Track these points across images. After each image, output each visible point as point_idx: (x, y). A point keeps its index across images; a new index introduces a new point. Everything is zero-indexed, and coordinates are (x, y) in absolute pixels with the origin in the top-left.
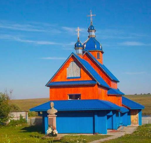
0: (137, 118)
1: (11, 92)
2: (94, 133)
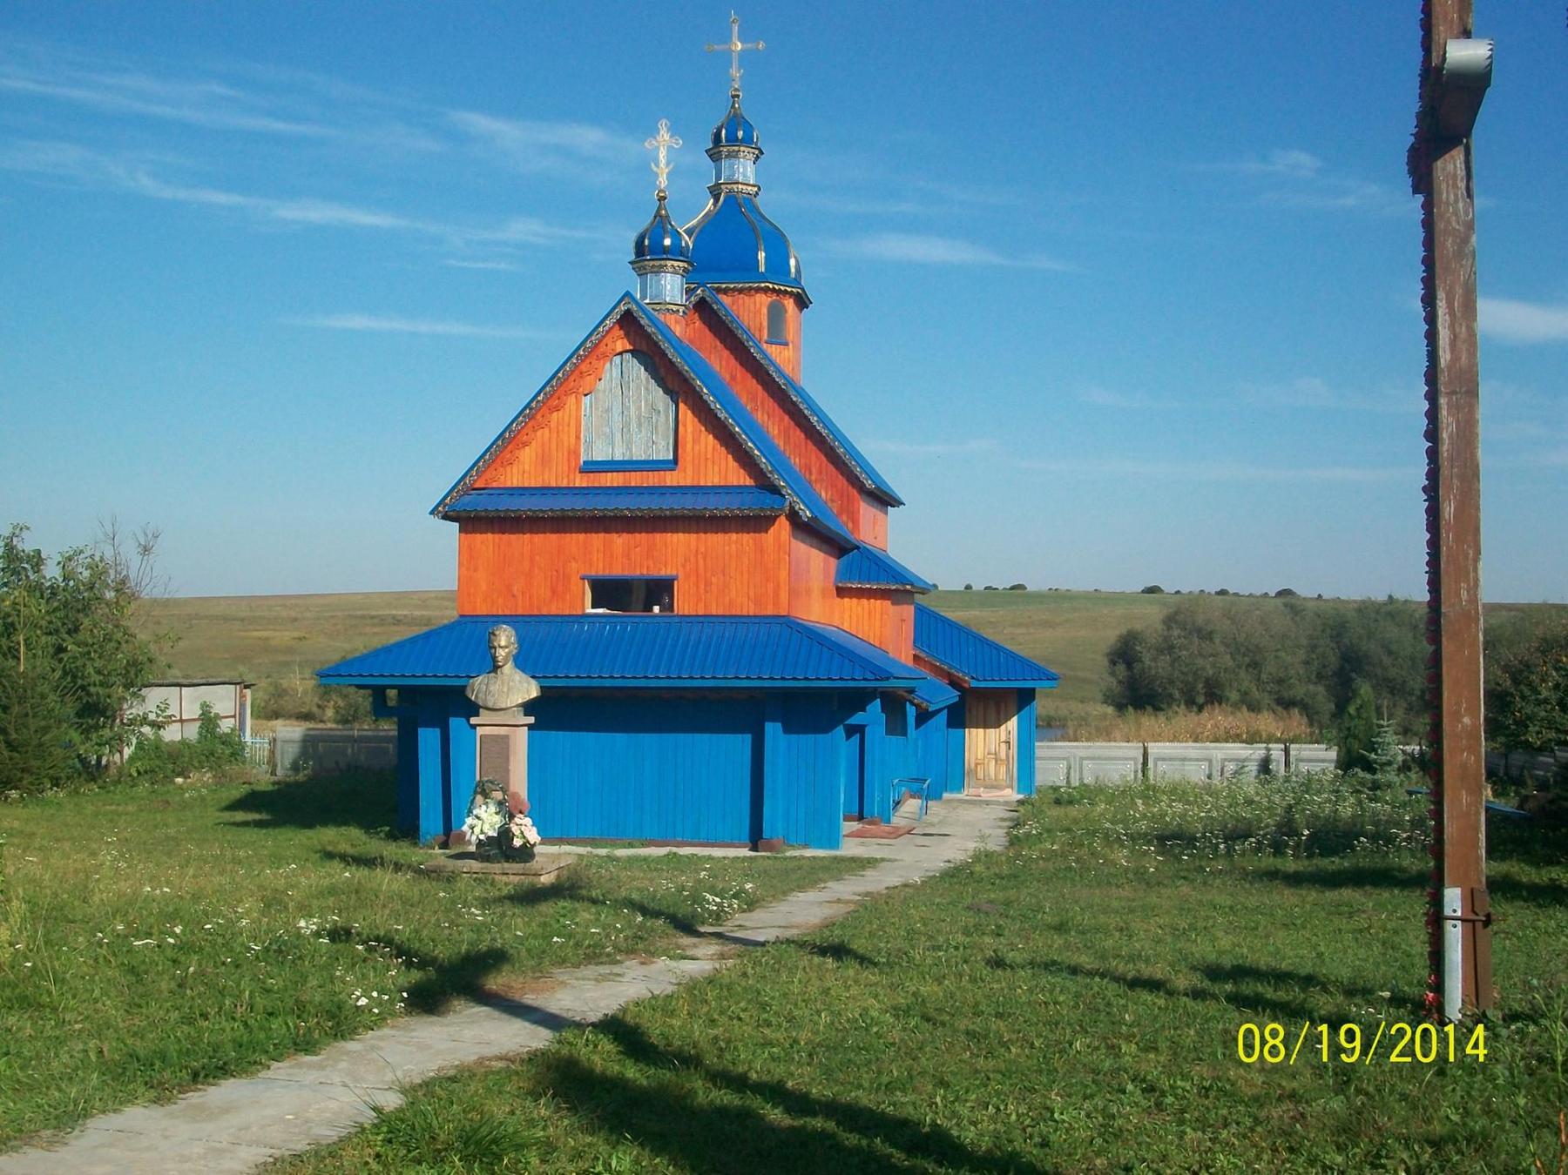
0: (1003, 746)
1: (146, 550)
2: (756, 839)
